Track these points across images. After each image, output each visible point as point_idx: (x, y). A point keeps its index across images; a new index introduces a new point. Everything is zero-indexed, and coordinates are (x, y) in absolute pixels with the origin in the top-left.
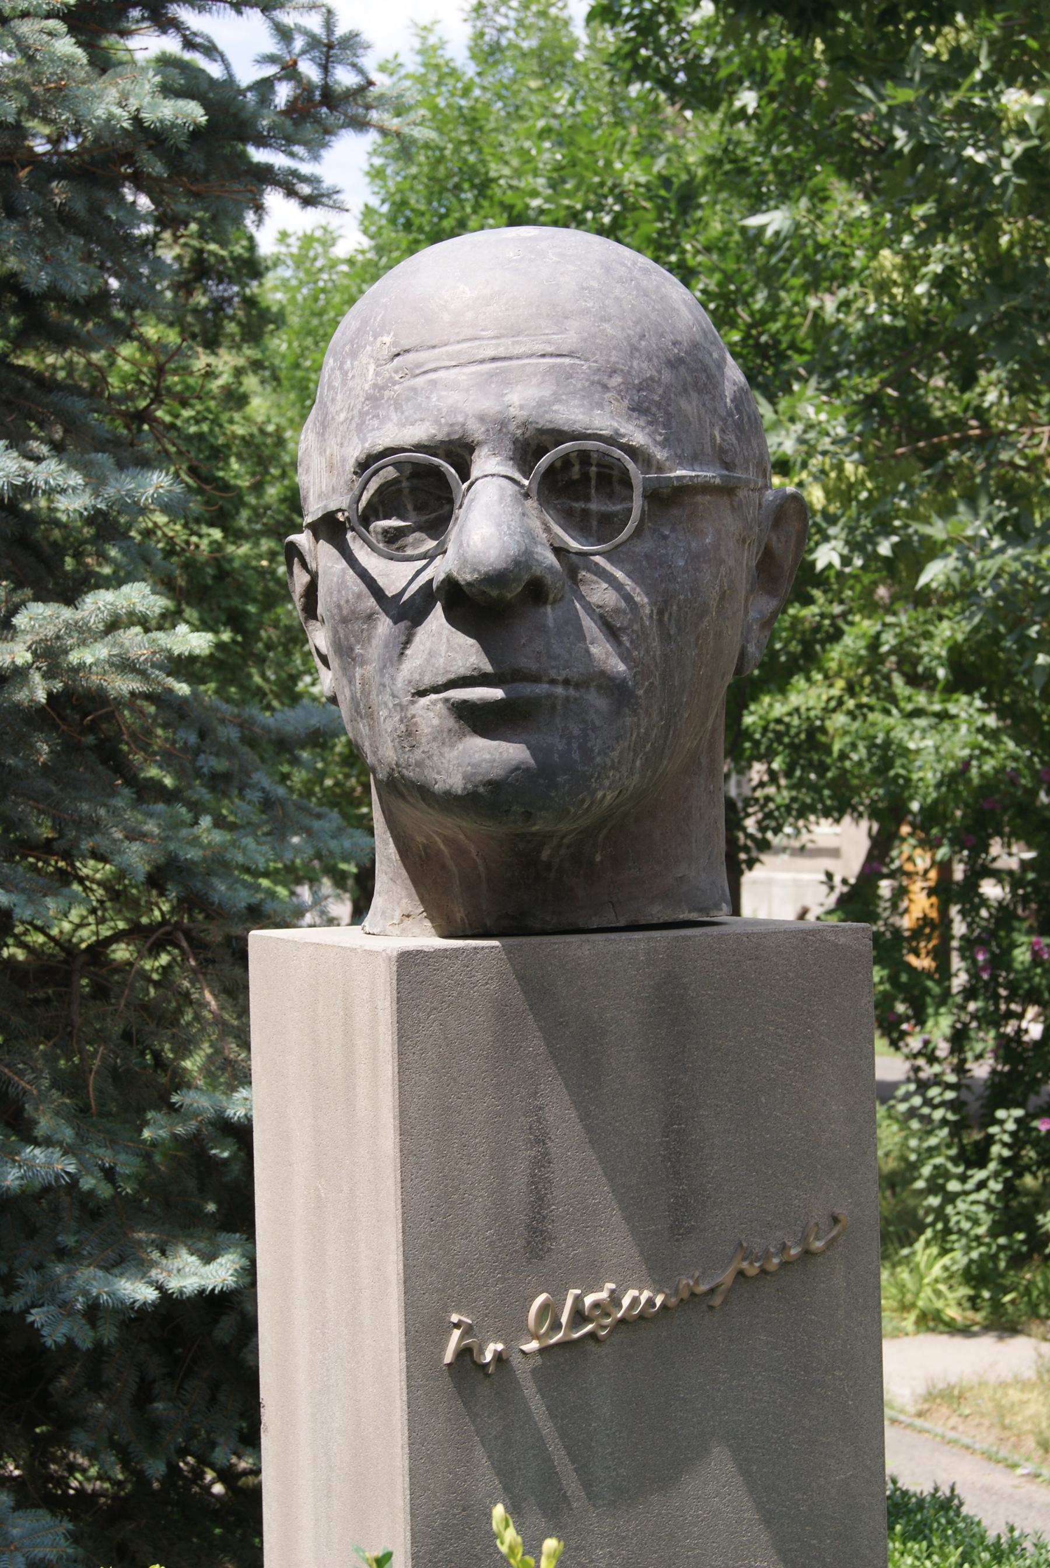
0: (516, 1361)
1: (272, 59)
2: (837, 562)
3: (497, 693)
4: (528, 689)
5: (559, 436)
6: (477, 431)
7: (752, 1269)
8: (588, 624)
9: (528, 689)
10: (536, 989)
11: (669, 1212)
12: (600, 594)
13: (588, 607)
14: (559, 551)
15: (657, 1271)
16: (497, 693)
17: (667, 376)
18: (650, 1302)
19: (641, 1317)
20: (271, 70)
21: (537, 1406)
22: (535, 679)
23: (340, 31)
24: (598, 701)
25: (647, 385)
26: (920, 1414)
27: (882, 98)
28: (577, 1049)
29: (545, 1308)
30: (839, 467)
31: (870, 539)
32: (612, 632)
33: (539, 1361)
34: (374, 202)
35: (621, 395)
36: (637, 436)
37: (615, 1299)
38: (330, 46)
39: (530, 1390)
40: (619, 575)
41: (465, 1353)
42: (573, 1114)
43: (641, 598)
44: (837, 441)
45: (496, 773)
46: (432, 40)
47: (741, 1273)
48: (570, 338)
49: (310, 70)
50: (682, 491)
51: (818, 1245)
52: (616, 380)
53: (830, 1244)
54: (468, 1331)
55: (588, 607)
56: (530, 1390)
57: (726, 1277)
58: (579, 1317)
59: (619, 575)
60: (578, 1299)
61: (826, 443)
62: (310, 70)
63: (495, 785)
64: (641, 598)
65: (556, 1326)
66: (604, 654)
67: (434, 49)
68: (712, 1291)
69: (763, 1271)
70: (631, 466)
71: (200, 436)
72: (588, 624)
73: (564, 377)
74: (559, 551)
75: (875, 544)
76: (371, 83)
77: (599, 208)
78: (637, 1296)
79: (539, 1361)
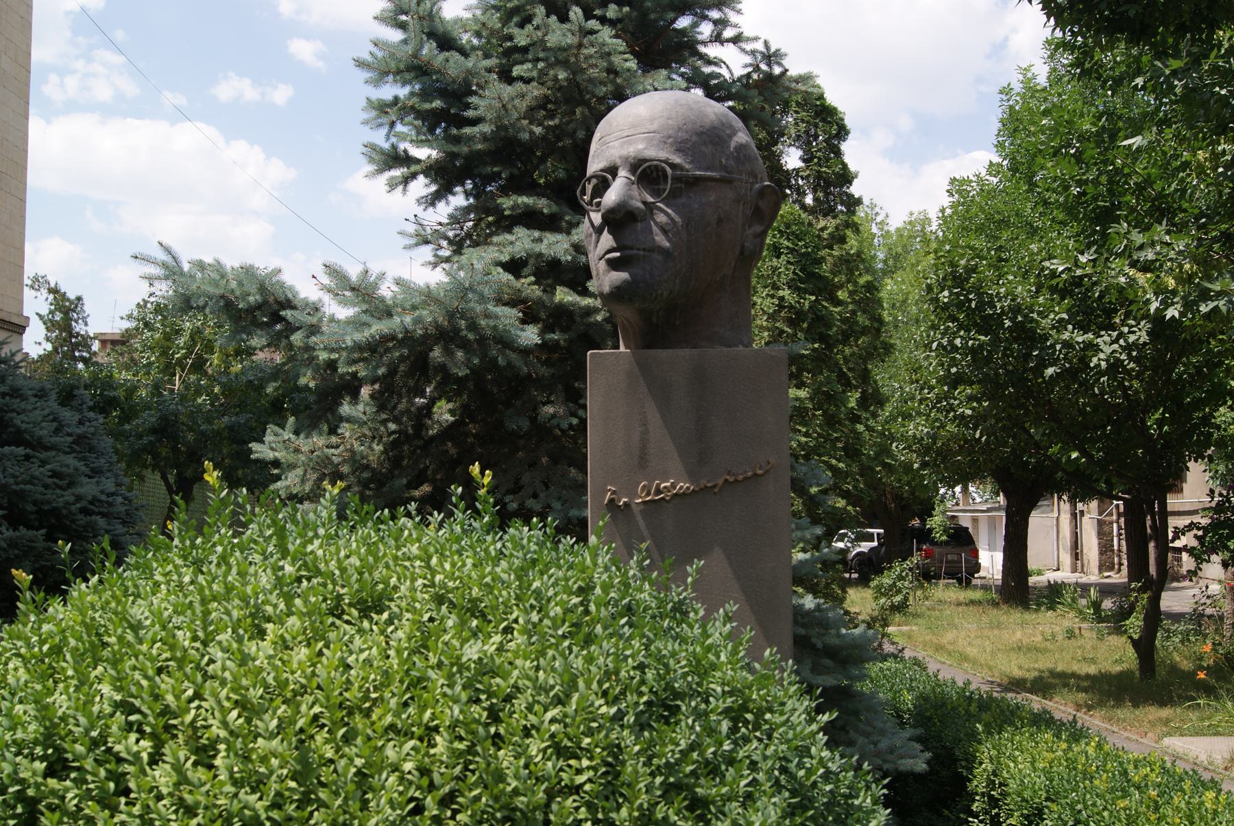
0: (633, 506)
1: (751, 65)
2: (1177, 315)
3: (618, 254)
4: (628, 252)
5: (645, 161)
6: (619, 162)
7: (731, 479)
8: (655, 228)
9: (628, 252)
10: (644, 368)
11: (697, 454)
12: (661, 218)
13: (656, 223)
14: (645, 203)
15: (692, 476)
16: (618, 254)
17: (694, 138)
18: (688, 488)
19: (684, 494)
20: (750, 69)
21: (642, 523)
22: (632, 248)
23: (773, 50)
24: (658, 257)
25: (685, 141)
26: (1226, 769)
27: (1167, 66)
28: (660, 391)
29: (644, 486)
30: (1181, 266)
31: (1196, 303)
32: (664, 231)
33: (642, 507)
34: (996, 159)
35: (671, 145)
36: (677, 159)
37: (673, 486)
38: (770, 56)
39: (639, 518)
40: (669, 211)
41: (612, 501)
42: (658, 415)
43: (677, 219)
44: (1180, 253)
45: (618, 283)
46: (1029, 75)
47: (726, 480)
48: (655, 126)
49: (764, 67)
50: (698, 180)
51: (760, 472)
52: (671, 140)
53: (767, 472)
54: (614, 492)
55: (656, 223)
56: (639, 518)
57: (720, 482)
58: (658, 492)
59: (669, 211)
60: (658, 485)
61: (1172, 255)
62: (764, 67)
63: (618, 288)
64: (677, 219)
65: (648, 494)
66: (661, 240)
67: (1030, 80)
68: (715, 486)
69: (736, 480)
70: (668, 169)
71: (807, 254)
72: (655, 228)
73: (650, 140)
74: (645, 203)
75: (1198, 306)
76: (787, 70)
77: (1069, 145)
78: (683, 485)
79: (642, 507)
